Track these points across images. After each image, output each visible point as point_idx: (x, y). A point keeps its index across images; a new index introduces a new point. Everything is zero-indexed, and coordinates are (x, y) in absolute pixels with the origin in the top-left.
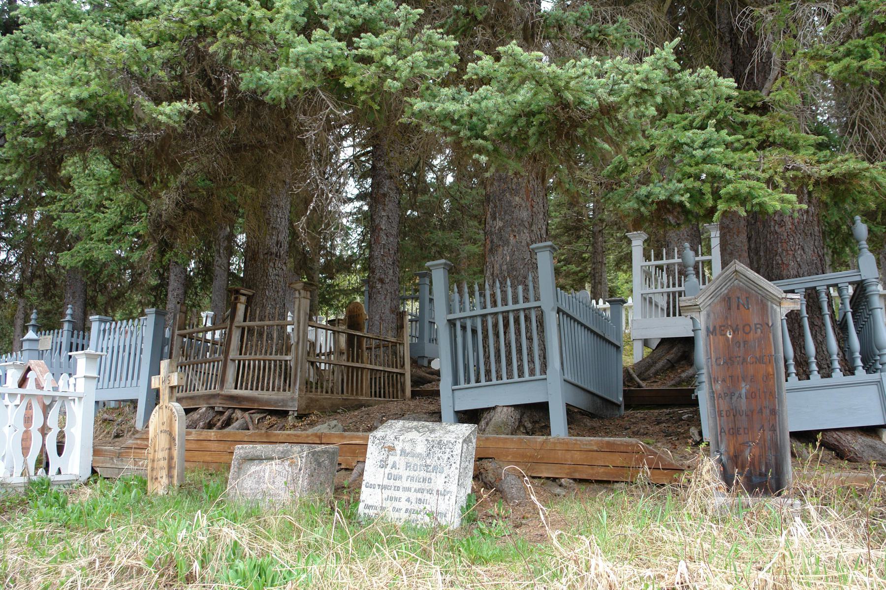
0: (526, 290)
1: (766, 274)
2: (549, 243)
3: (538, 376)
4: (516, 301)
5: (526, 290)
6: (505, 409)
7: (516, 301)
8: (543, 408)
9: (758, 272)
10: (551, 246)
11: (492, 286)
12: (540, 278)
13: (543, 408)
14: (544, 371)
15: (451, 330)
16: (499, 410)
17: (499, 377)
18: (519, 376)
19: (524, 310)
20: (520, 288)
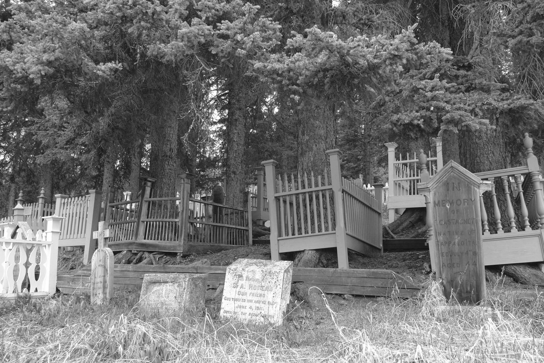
0: (323, 178)
2: (338, 150)
4: (317, 186)
5: (323, 178)
6: (310, 252)
8: (333, 251)
10: (338, 151)
13: (333, 251)
14: (334, 228)
16: (306, 252)
17: (306, 232)
18: (319, 232)
19: (322, 190)
20: (320, 177)
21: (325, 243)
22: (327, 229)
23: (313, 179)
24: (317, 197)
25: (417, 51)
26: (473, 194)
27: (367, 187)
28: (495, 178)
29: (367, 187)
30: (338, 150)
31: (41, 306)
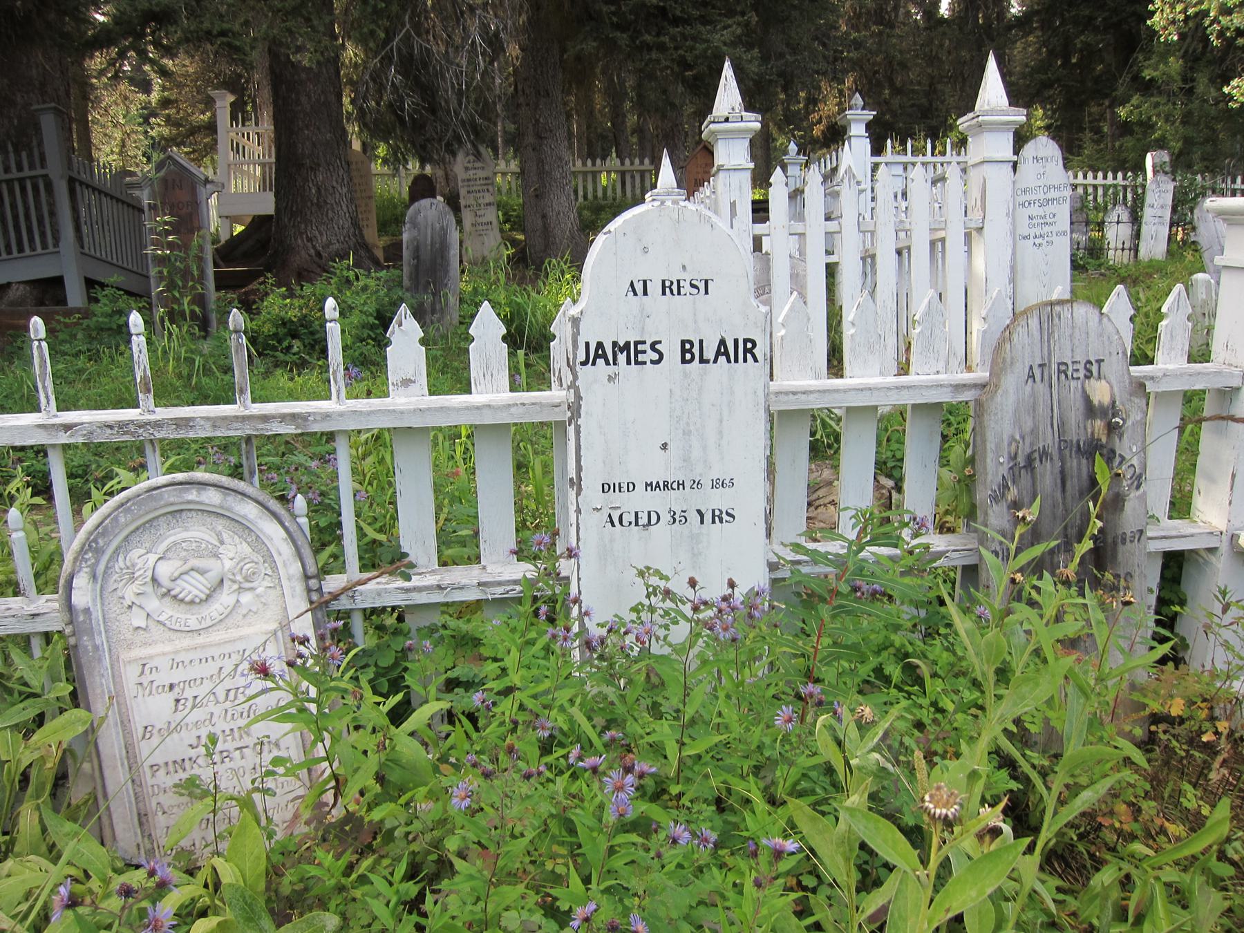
0: (30, 156)
1: (1180, 197)
2: (53, 105)
3: (51, 249)
4: (20, 169)
5: (30, 156)
6: (22, 287)
7: (20, 169)
8: (58, 282)
9: (298, 399)
10: (55, 108)
11: (235, 179)
12: (809, 278)
13: (58, 282)
14: (56, 245)
15: (991, 131)
16: (14, 287)
17: (21, 250)
18: (43, 249)
19: (31, 178)
20: (24, 154)
21: (42, 269)
22: (44, 246)
23: (12, 156)
24: (36, 189)
25: (317, 336)
26: (180, 476)
27: (632, 163)
28: (842, 377)
29: (632, 163)
30: (53, 105)
31: (513, 104)
